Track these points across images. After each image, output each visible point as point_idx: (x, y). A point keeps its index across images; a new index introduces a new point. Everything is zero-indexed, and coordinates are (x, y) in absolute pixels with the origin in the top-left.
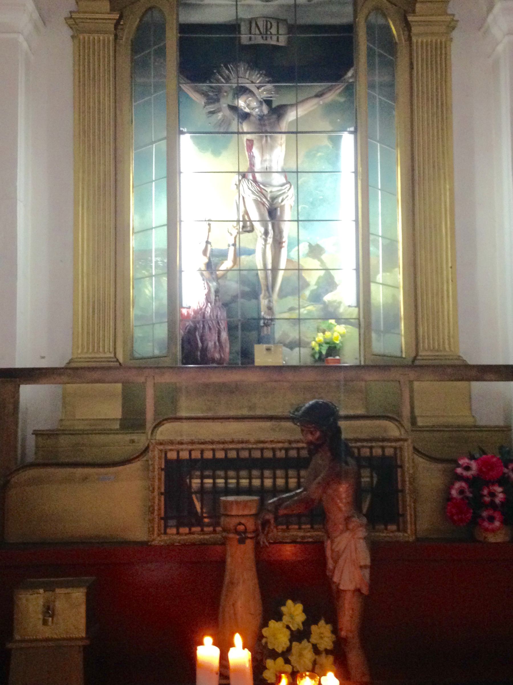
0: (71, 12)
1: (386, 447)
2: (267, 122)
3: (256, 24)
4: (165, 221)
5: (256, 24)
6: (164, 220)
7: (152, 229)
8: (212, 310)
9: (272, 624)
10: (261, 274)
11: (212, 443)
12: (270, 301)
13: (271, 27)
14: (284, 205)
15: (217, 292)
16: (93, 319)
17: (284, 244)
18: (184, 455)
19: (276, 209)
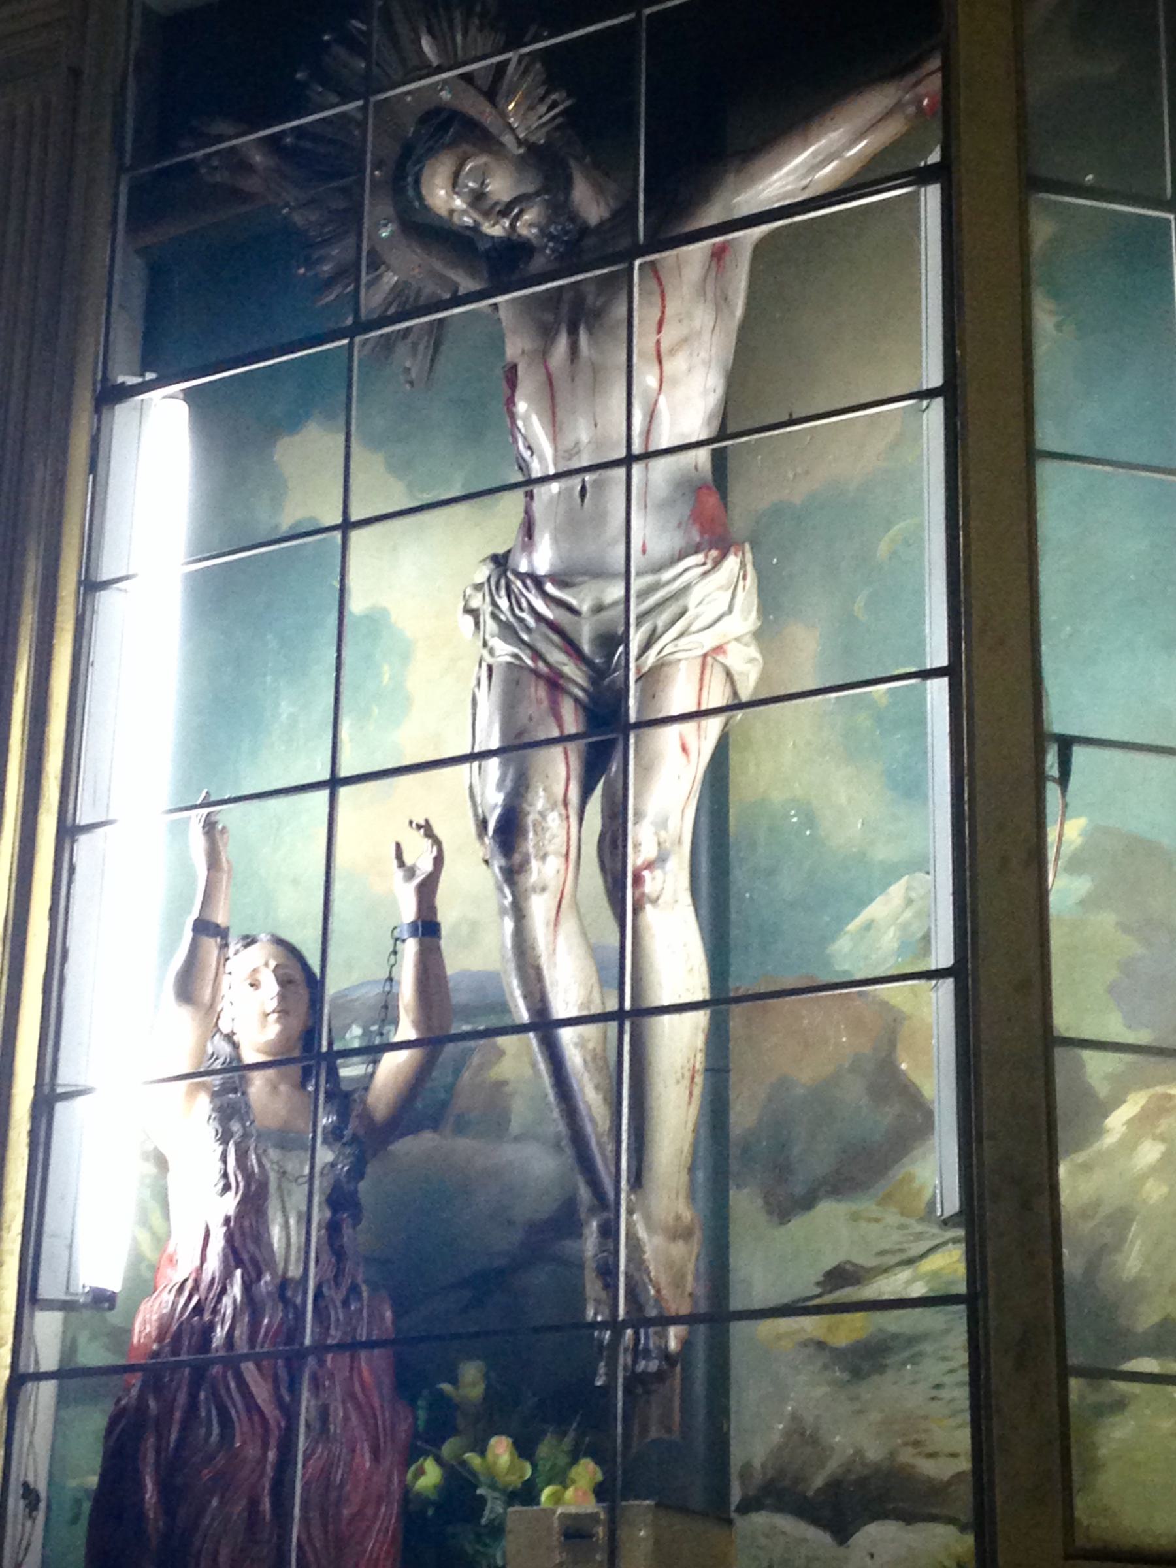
8: (251, 1301)
14: (660, 666)
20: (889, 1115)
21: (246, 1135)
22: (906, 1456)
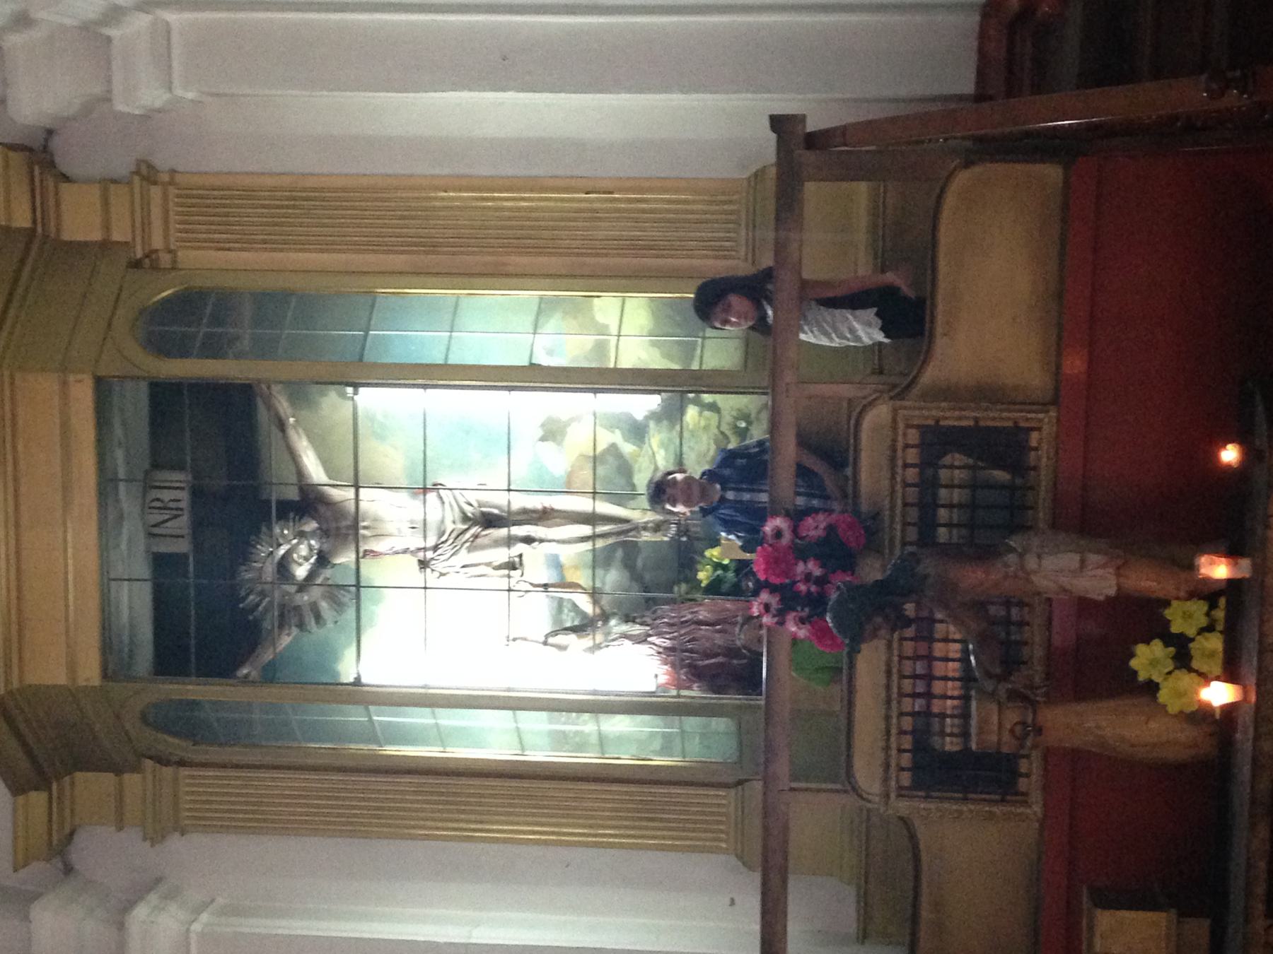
0: (145, 839)
1: (903, 538)
2: (334, 525)
3: (154, 526)
4: (510, 713)
5: (154, 526)
6: (508, 714)
7: (518, 729)
8: (659, 634)
9: (1163, 696)
10: (600, 543)
11: (887, 718)
12: (645, 529)
13: (158, 500)
14: (478, 501)
15: (628, 619)
16: (668, 820)
17: (547, 505)
18: (906, 759)
19: (483, 514)
20: (610, 459)
21: (606, 641)
22: (709, 458)
